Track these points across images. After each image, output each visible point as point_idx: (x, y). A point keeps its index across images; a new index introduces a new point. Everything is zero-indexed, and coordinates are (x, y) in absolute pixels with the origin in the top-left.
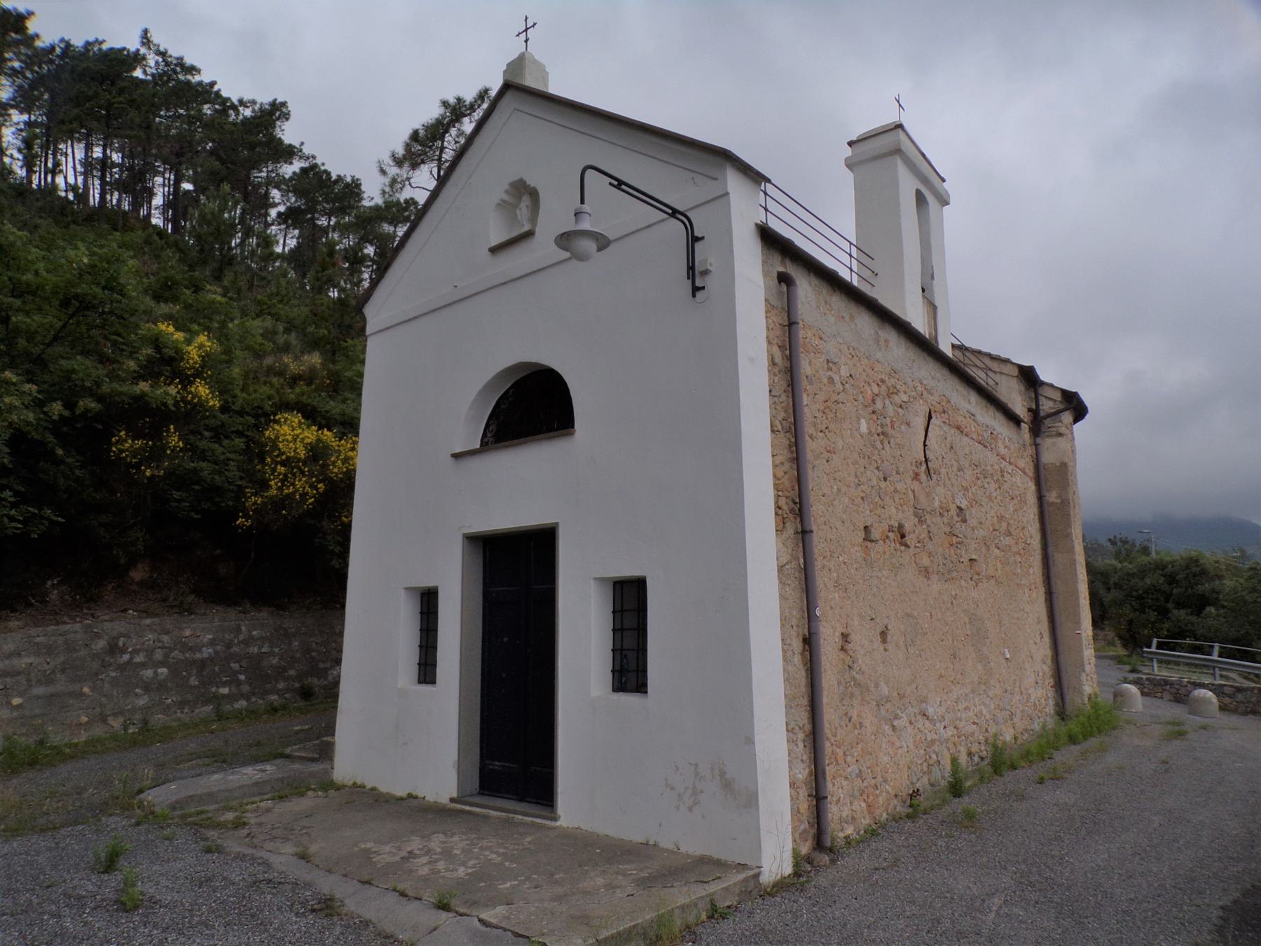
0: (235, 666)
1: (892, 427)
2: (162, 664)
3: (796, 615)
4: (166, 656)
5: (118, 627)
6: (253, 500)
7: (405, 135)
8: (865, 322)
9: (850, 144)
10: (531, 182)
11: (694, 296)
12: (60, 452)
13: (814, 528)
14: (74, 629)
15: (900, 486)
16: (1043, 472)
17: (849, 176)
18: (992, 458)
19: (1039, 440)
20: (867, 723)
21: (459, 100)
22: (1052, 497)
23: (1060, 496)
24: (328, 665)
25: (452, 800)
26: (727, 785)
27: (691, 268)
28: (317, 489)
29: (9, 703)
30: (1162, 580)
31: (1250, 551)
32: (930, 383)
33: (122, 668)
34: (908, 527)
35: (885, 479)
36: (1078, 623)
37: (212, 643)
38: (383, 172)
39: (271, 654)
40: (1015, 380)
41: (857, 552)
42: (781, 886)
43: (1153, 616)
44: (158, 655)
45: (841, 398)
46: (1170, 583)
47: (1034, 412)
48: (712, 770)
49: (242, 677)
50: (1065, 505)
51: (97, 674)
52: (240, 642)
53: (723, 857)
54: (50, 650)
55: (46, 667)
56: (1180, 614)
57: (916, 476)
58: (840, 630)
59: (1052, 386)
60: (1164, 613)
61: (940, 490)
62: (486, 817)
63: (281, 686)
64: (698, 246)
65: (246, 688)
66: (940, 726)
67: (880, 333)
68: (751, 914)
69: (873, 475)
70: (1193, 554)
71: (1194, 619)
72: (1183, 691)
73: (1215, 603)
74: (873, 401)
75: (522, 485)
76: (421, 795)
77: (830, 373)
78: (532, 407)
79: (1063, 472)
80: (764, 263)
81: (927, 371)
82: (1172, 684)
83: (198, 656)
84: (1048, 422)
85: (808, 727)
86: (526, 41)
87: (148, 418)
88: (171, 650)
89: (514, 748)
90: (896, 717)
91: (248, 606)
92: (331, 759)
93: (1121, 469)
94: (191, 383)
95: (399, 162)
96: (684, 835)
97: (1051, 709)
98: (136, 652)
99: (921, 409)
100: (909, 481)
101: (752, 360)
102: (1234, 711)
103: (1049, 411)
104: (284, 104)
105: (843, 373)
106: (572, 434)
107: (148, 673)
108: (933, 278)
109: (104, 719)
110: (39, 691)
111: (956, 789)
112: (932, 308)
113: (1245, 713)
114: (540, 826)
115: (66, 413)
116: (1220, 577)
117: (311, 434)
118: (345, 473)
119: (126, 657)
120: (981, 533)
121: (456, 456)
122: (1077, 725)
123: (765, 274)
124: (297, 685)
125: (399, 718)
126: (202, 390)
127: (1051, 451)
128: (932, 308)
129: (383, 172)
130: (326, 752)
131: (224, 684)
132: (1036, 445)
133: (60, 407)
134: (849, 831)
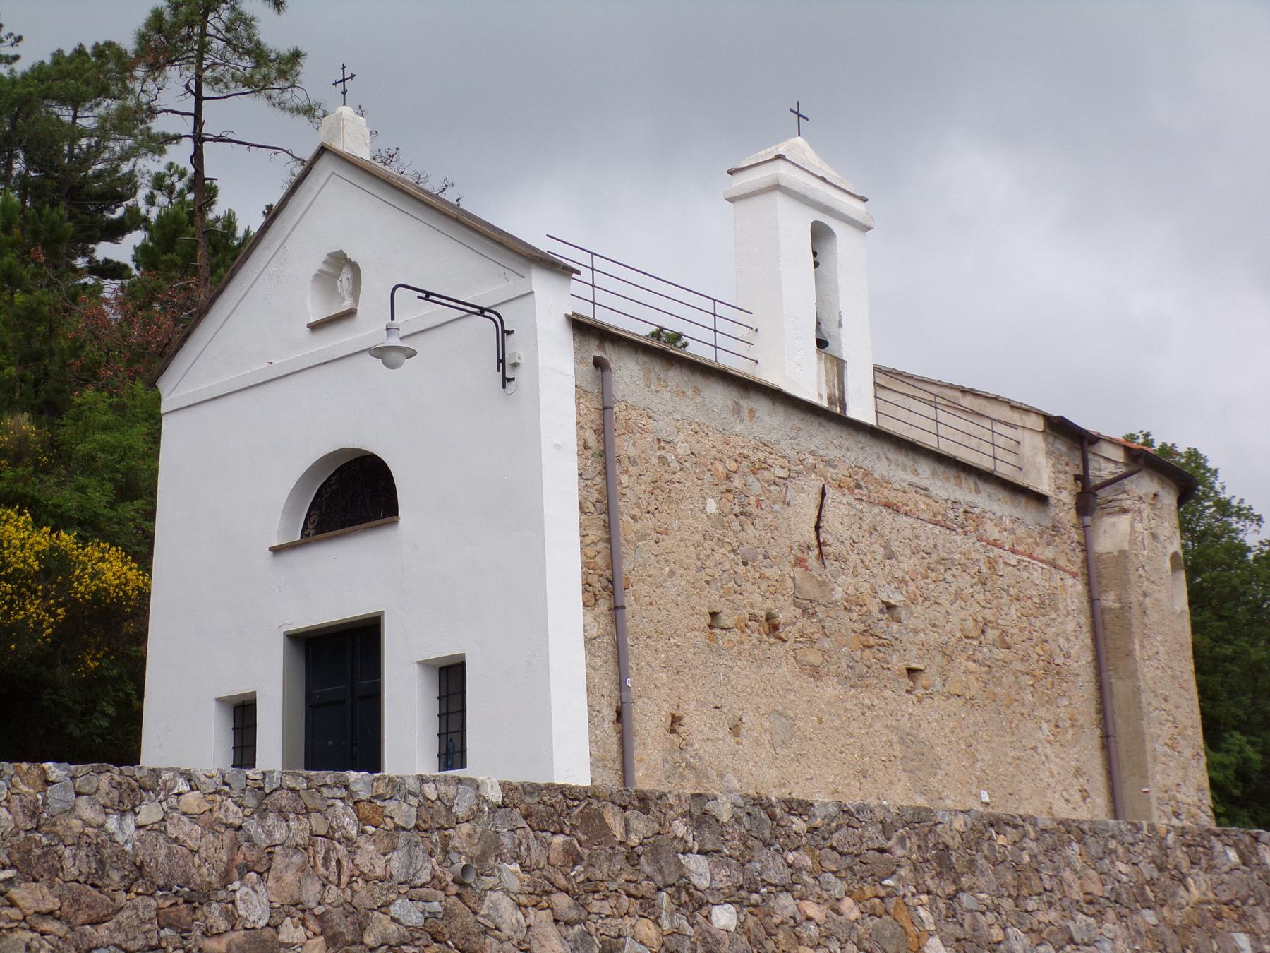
1: (759, 505)
3: (608, 686)
8: (718, 396)
11: (504, 387)
22: (1109, 600)
23: (1119, 599)
27: (501, 361)
28: (54, 615)
32: (832, 453)
34: (782, 617)
35: (745, 564)
40: (1040, 438)
41: (701, 639)
58: (667, 709)
64: (508, 339)
67: (743, 403)
74: (728, 477)
75: (344, 577)
77: (662, 452)
78: (353, 494)
80: (576, 351)
86: (344, 93)
99: (812, 484)
100: (787, 568)
105: (680, 451)
106: (396, 522)
108: (840, 325)
117: (42, 539)
118: (95, 593)
123: (579, 360)
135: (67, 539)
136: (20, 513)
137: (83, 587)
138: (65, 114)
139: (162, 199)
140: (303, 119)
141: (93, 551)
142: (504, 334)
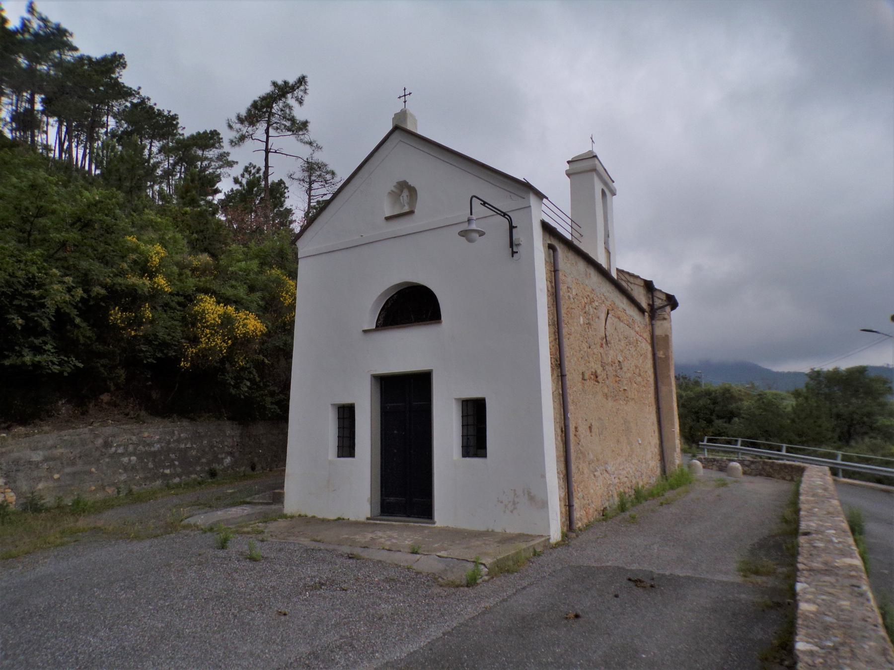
0: (172, 456)
2: (134, 454)
4: (135, 449)
5: (108, 430)
6: (192, 351)
7: (248, 104)
9: (568, 162)
10: (411, 183)
12: (78, 320)
13: (567, 373)
14: (84, 431)
15: (595, 351)
16: (656, 341)
17: (568, 180)
18: (633, 333)
19: (654, 322)
20: (585, 472)
21: (285, 82)
22: (660, 354)
23: (664, 354)
24: (223, 456)
25: (368, 519)
26: (532, 498)
29: (52, 477)
30: (709, 401)
31: (757, 384)
32: (607, 294)
33: (112, 456)
34: (599, 372)
36: (673, 425)
37: (159, 441)
38: (230, 127)
39: (191, 448)
42: (558, 545)
43: (703, 423)
44: (131, 448)
45: (573, 306)
46: (714, 404)
47: (651, 306)
48: (524, 492)
49: (177, 463)
50: (667, 358)
51: (98, 460)
52: (174, 441)
53: (529, 533)
54: (73, 444)
55: (71, 455)
56: (719, 423)
57: (602, 346)
59: (660, 291)
60: (710, 422)
61: (611, 352)
62: (393, 525)
63: (198, 468)
64: (514, 230)
65: (179, 470)
66: (613, 477)
68: (551, 554)
69: (585, 346)
70: (727, 386)
71: (726, 425)
72: (723, 465)
73: (738, 415)
75: (406, 350)
76: (346, 518)
78: (411, 306)
79: (666, 339)
81: (606, 289)
82: (718, 461)
83: (152, 449)
84: (659, 312)
85: (564, 472)
87: (131, 299)
88: (138, 445)
89: (405, 487)
90: (596, 471)
91: (176, 419)
92: (283, 503)
93: (691, 334)
94: (156, 276)
95: (241, 120)
96: (511, 525)
97: (658, 472)
98: (118, 446)
99: (604, 309)
101: (541, 290)
102: (750, 474)
103: (655, 304)
104: (121, 56)
107: (125, 460)
109: (103, 488)
110: (68, 470)
111: (622, 508)
112: (608, 252)
113: (756, 475)
114: (427, 527)
115: (85, 296)
116: (741, 400)
117: (220, 309)
118: (244, 334)
119: (113, 449)
120: (629, 375)
121: (365, 331)
122: (671, 481)
124: (207, 468)
125: (326, 476)
126: (161, 281)
127: (660, 328)
128: (608, 252)
129: (230, 127)
130: (278, 498)
131: (168, 467)
132: (652, 325)
133: (81, 292)
134: (580, 525)
135: (230, 309)
136: (211, 297)
137: (239, 332)
138: (200, 153)
139: (247, 176)
140: (308, 146)
141: (242, 315)
142: (512, 228)
